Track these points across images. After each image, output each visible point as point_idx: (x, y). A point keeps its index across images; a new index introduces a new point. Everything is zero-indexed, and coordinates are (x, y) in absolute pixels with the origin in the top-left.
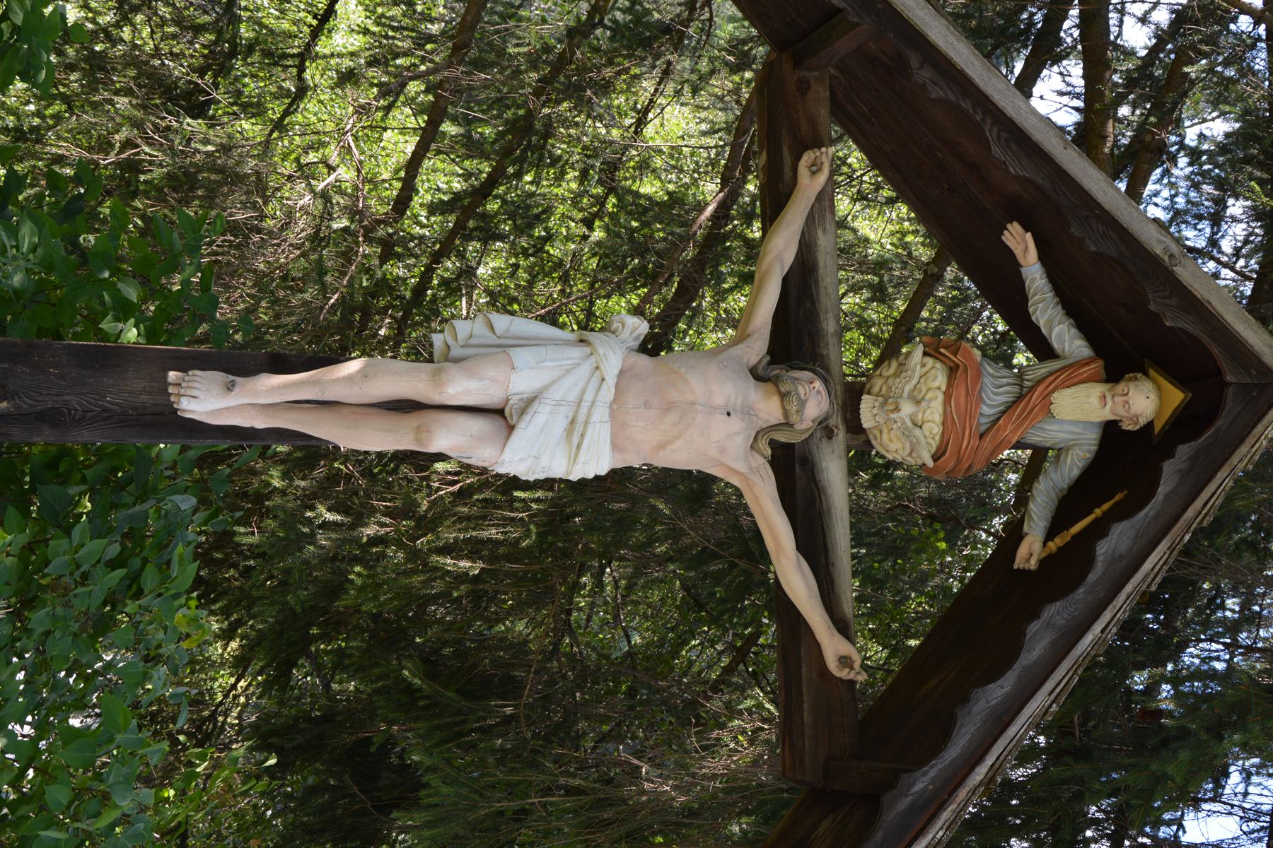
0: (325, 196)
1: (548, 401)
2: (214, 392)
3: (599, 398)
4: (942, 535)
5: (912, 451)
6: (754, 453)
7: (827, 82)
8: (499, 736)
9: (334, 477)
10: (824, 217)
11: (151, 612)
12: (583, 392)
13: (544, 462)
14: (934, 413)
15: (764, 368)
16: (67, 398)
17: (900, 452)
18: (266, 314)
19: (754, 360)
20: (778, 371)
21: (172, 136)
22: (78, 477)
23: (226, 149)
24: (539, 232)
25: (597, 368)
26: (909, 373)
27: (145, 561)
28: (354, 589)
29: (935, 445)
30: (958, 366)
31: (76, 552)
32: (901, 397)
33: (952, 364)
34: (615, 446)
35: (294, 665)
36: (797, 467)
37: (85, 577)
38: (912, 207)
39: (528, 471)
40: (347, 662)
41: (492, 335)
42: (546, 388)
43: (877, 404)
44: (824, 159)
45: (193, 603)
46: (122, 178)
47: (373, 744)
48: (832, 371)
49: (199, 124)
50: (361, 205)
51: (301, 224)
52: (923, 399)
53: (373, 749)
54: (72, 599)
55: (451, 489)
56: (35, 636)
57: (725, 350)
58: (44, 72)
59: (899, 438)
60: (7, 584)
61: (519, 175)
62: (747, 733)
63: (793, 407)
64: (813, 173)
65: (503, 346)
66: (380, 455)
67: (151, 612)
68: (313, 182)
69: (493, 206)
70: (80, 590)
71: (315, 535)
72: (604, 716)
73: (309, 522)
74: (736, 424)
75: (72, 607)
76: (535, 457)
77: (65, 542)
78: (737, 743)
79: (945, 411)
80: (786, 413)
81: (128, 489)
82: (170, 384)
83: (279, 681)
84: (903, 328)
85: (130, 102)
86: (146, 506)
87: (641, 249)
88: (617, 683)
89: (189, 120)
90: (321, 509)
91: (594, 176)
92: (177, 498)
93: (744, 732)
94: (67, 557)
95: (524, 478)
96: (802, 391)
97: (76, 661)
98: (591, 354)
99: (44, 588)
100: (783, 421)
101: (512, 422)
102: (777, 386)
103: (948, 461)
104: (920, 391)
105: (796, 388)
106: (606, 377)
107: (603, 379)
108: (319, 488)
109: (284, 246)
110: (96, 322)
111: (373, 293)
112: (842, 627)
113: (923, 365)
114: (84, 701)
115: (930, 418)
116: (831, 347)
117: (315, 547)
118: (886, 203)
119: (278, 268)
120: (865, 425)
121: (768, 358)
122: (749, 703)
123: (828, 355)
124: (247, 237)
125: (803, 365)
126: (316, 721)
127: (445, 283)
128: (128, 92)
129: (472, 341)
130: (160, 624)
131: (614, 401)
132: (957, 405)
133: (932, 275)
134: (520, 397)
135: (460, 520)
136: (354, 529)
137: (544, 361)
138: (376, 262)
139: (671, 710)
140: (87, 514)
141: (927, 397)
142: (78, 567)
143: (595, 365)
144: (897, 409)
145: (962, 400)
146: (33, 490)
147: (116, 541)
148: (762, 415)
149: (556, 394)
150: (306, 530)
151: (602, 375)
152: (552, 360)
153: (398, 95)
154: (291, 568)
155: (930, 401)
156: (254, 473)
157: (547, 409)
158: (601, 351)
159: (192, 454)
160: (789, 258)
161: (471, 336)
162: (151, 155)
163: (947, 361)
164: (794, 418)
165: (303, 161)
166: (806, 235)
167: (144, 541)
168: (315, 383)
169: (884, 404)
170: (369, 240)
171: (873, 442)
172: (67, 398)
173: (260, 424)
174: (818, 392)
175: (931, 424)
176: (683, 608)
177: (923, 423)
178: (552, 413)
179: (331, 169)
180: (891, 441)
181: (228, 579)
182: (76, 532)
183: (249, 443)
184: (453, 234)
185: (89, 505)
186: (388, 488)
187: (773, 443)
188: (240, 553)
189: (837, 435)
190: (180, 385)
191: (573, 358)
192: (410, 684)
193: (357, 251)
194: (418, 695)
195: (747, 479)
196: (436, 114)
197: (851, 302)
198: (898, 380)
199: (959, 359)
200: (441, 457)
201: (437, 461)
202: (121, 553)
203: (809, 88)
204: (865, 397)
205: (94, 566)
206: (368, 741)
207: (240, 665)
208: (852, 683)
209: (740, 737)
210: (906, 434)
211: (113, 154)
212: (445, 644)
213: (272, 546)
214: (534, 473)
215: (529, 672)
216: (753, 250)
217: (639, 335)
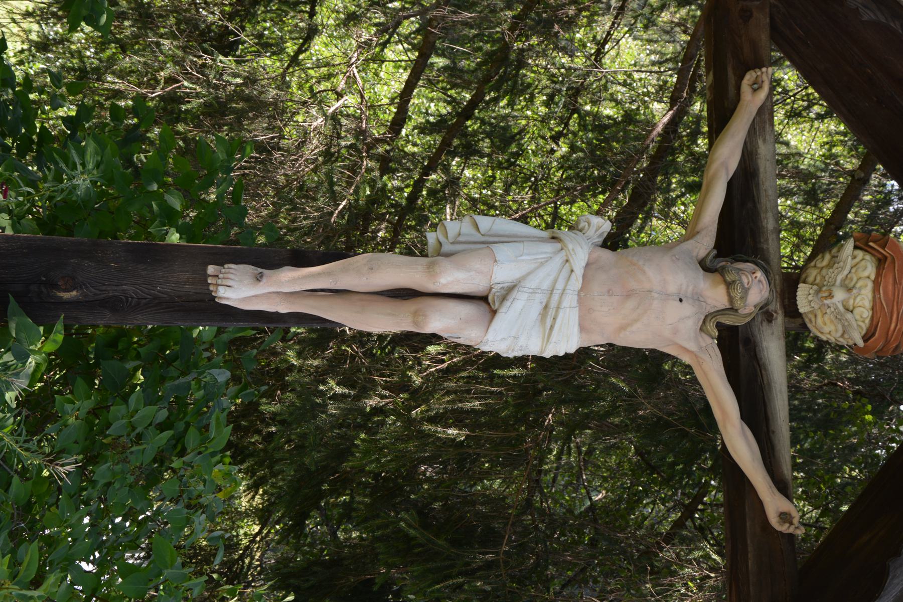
0: (334, 118)
1: (525, 289)
2: (245, 282)
3: (568, 287)
4: (869, 407)
5: (844, 333)
6: (703, 334)
7: (768, 10)
8: (480, 578)
9: (340, 357)
10: (764, 128)
11: (192, 467)
12: (555, 281)
13: (522, 341)
14: (864, 299)
15: (711, 261)
16: (125, 287)
17: (833, 333)
18: (285, 219)
19: (702, 253)
20: (724, 263)
21: (207, 71)
22: (134, 353)
23: (250, 80)
24: (514, 149)
25: (567, 261)
26: (841, 264)
27: (188, 425)
28: (360, 452)
29: (865, 327)
30: (886, 258)
31: (132, 417)
32: (833, 285)
33: (880, 256)
34: (582, 328)
35: (308, 517)
36: (741, 348)
37: (139, 437)
38: (847, 122)
39: (508, 350)
40: (354, 514)
41: (477, 233)
42: (524, 278)
43: (812, 292)
44: (765, 78)
45: (227, 460)
46: (164, 109)
47: (375, 584)
48: (772, 263)
49: (230, 61)
50: (364, 126)
51: (315, 141)
52: (854, 287)
53: (375, 588)
54: (129, 456)
55: (440, 366)
56: (99, 486)
57: (677, 245)
58: (105, 16)
59: (832, 321)
60: (76, 442)
61: (496, 100)
62: (695, 580)
63: (737, 294)
64: (755, 90)
65: (488, 243)
66: (381, 337)
67: (192, 467)
68: (325, 108)
69: (472, 125)
70: (135, 448)
71: (327, 405)
72: (570, 562)
73: (322, 394)
74: (687, 309)
75: (129, 462)
76: (515, 337)
77: (122, 409)
78: (687, 589)
79: (874, 297)
80: (731, 299)
81: (174, 364)
82: (210, 276)
83: (296, 530)
84: (833, 227)
85: (172, 43)
86: (188, 378)
87: (601, 163)
88: (581, 534)
89: (221, 57)
90: (332, 383)
91: (561, 100)
92: (215, 372)
93: (693, 579)
94: (124, 421)
95: (505, 355)
96: (745, 280)
97: (131, 508)
98: (562, 249)
99: (105, 446)
100: (728, 307)
101: (494, 307)
102: (723, 276)
103: (878, 341)
104: (852, 280)
105: (740, 277)
106: (575, 269)
107: (572, 271)
108: (329, 366)
109: (301, 161)
110: (145, 227)
111: (372, 201)
112: (782, 487)
113: (854, 257)
114: (137, 542)
115: (860, 304)
116: (770, 241)
117: (327, 415)
118: (816, 119)
119: (296, 180)
120: (801, 310)
121: (715, 252)
122: (697, 554)
123: (768, 249)
124: (269, 153)
125: (746, 258)
126: (324, 564)
127: (432, 193)
128: (172, 36)
129: (461, 239)
130: (200, 478)
131: (582, 289)
132: (885, 293)
133: (859, 180)
134: (501, 286)
135: (448, 393)
136: (359, 400)
137: (521, 256)
138: (377, 173)
139: (629, 558)
140: (141, 385)
141: (858, 285)
142: (134, 429)
143: (565, 258)
144: (830, 296)
145: (890, 287)
146: (97, 364)
147: (164, 408)
148: (709, 301)
149: (531, 283)
150: (318, 401)
151: (571, 266)
152: (528, 255)
153: (391, 36)
154: (305, 434)
155: (860, 289)
156: (275, 353)
157: (525, 296)
158: (570, 246)
159: (225, 337)
160: (733, 165)
161: (460, 234)
162: (191, 89)
163: (876, 254)
164: (738, 304)
165: (317, 88)
166: (748, 145)
167: (187, 408)
168: (329, 274)
169: (819, 291)
170: (371, 157)
171: (809, 325)
172: (125, 287)
173: (283, 309)
174: (760, 281)
175: (861, 309)
176: (635, 472)
177: (854, 308)
178: (528, 299)
179: (340, 95)
180: (825, 324)
181: (254, 443)
182: (133, 399)
183: (272, 326)
184: (440, 151)
185: (142, 377)
186: (387, 366)
187: (719, 326)
188: (263, 421)
189: (776, 319)
190: (217, 276)
191: (546, 253)
192: (407, 535)
193: (362, 165)
194: (414, 542)
195: (697, 357)
196: (425, 50)
197: (783, 204)
198: (831, 270)
199: (887, 252)
200: (434, 338)
201: (431, 344)
202: (168, 418)
203: (751, 16)
204: (801, 285)
205: (146, 428)
206: (371, 582)
207: (263, 516)
208: (791, 536)
209: (690, 584)
210: (839, 317)
211: (158, 88)
212: (436, 499)
213: (291, 414)
214: (513, 351)
215: (506, 524)
216: (699, 163)
217: (603, 233)
